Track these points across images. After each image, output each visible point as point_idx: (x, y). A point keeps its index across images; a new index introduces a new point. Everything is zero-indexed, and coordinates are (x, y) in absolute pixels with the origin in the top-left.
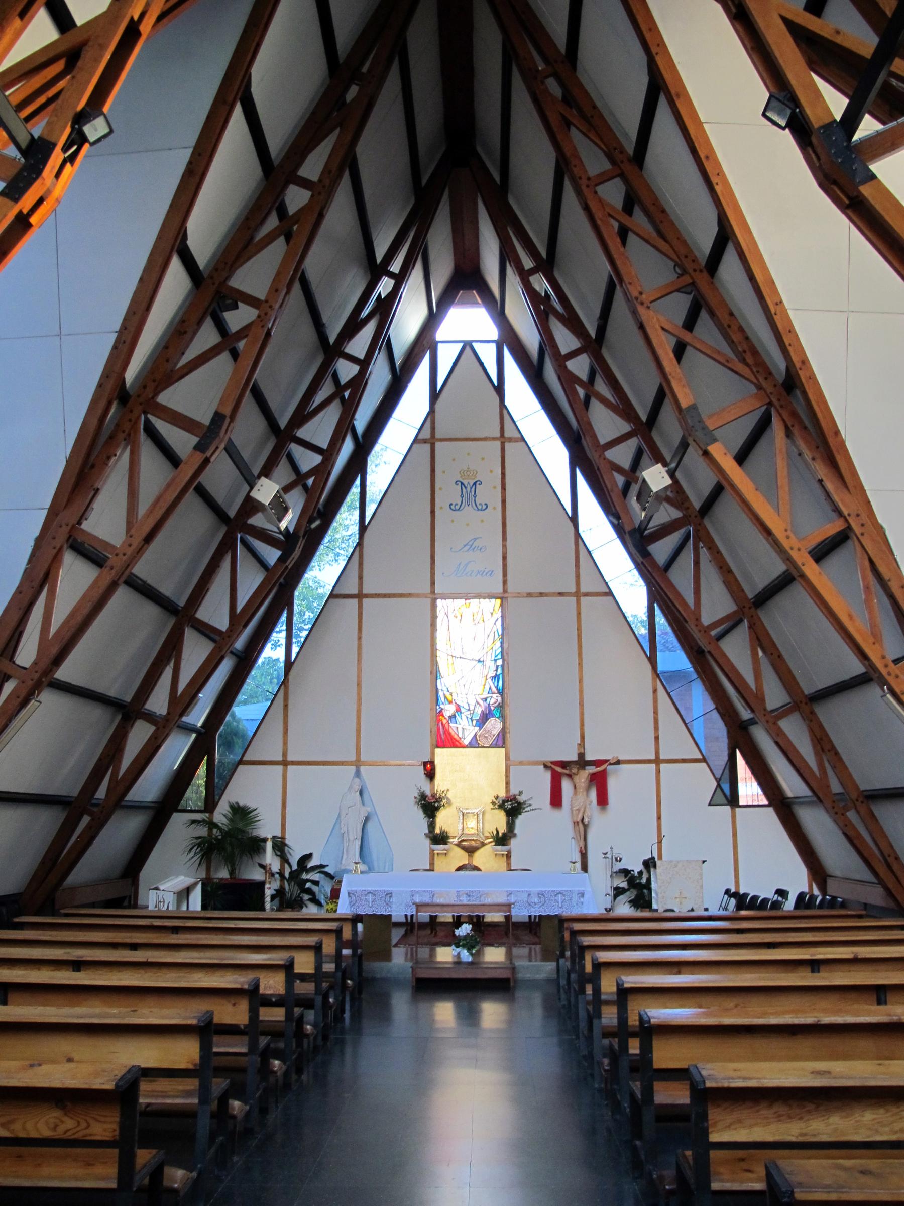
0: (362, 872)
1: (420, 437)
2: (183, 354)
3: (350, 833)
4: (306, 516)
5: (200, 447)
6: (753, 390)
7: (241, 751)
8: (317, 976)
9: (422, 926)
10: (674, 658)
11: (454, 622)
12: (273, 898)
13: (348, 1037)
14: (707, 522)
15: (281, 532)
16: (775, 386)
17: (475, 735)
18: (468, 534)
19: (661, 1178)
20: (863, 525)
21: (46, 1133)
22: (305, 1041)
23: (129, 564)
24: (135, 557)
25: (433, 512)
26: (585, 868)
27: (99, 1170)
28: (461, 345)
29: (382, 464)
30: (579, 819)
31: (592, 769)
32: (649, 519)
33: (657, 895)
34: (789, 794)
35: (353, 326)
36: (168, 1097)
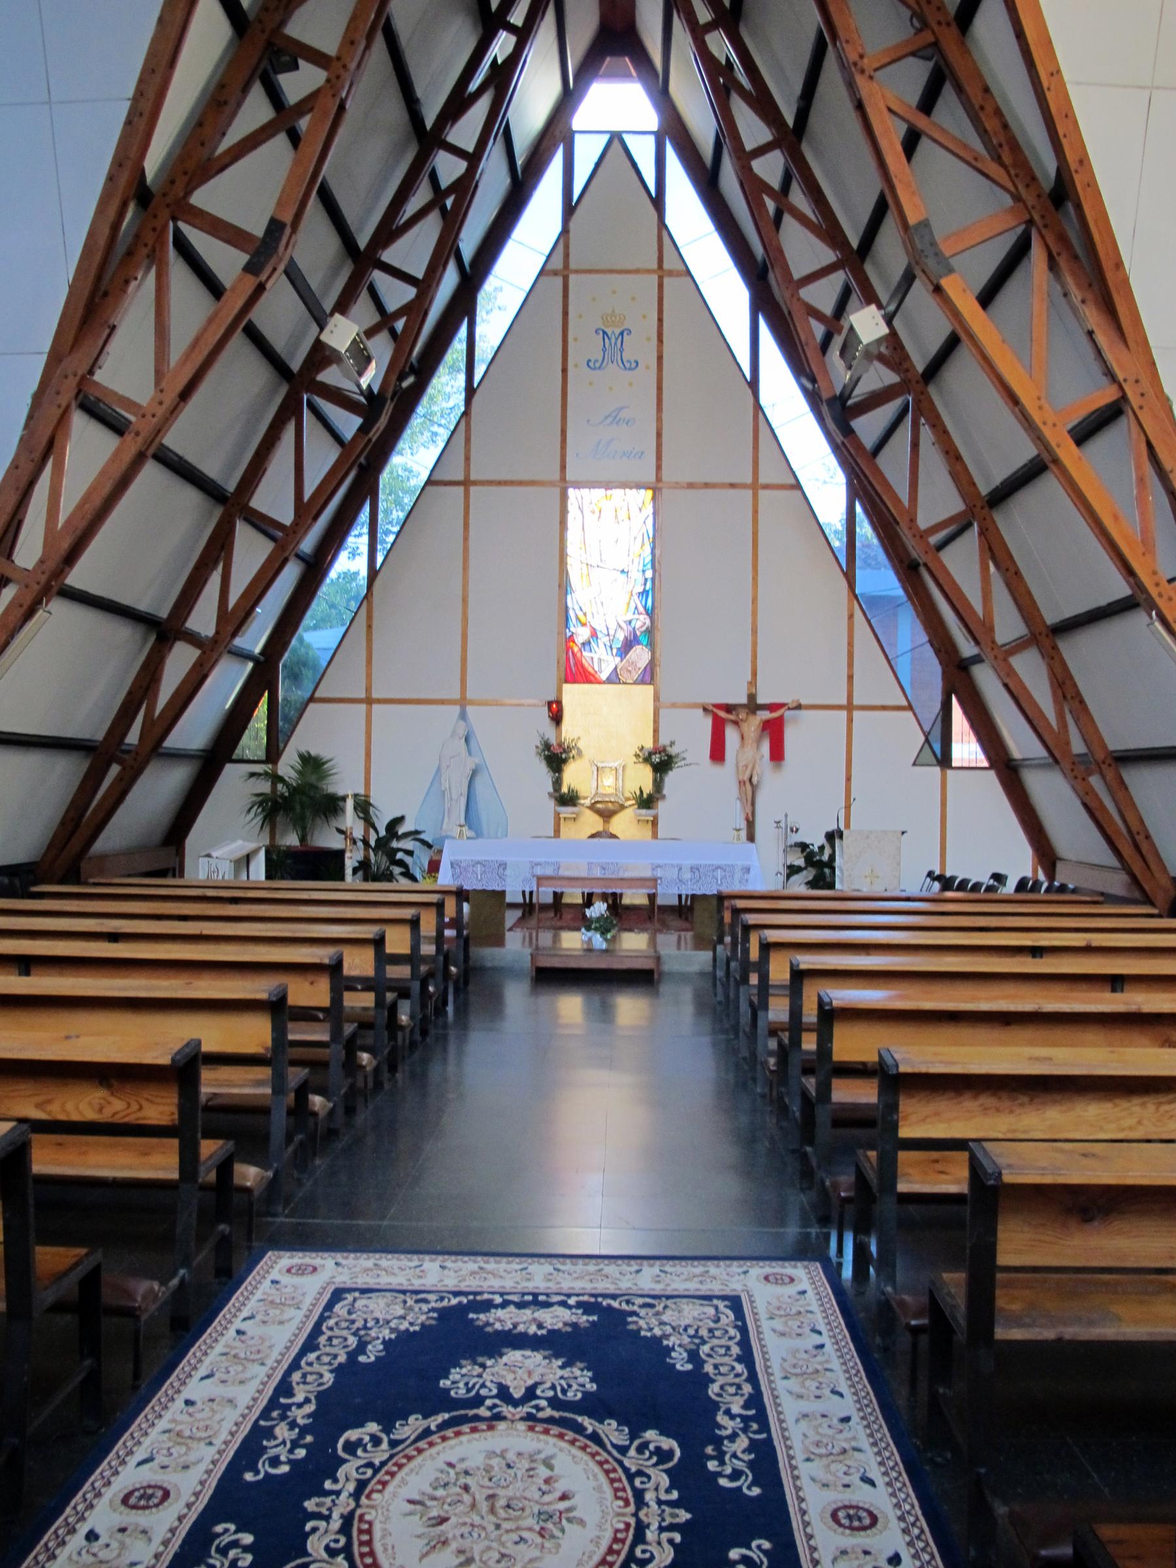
0: (468, 838)
1: (548, 267)
2: (224, 134)
3: (453, 792)
4: (396, 370)
5: (251, 268)
6: (1008, 201)
7: (312, 687)
8: (413, 958)
9: (544, 907)
10: (880, 579)
11: (590, 519)
12: (355, 871)
13: (452, 1034)
14: (932, 390)
15: (362, 393)
16: (1039, 196)
17: (616, 668)
18: (612, 400)
19: (835, 1186)
20: (1142, 395)
21: (90, 1115)
22: (400, 1034)
23: (159, 431)
24: (167, 419)
25: (564, 371)
26: (751, 838)
27: (157, 1159)
28: (606, 137)
29: (496, 311)
30: (746, 778)
31: (766, 715)
32: (855, 382)
33: (842, 871)
34: (1016, 753)
35: (458, 104)
36: (235, 1086)
